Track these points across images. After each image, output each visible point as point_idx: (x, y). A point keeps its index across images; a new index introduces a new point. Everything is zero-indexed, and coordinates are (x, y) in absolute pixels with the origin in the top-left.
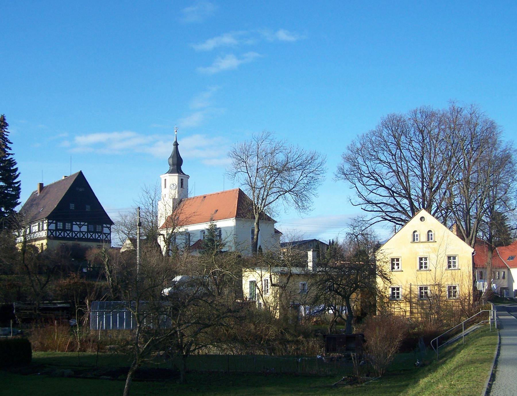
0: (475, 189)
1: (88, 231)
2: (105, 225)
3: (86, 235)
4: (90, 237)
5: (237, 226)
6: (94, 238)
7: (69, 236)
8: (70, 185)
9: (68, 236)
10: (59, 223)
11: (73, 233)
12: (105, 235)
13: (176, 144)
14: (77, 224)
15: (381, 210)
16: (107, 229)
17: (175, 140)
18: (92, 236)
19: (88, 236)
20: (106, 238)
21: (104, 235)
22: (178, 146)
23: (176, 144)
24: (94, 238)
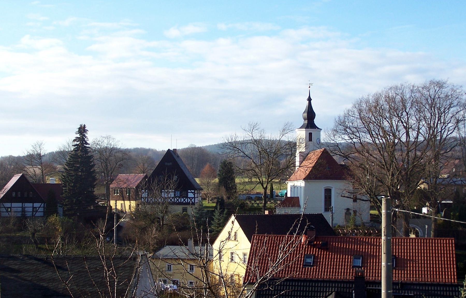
0: (434, 99)
1: (175, 197)
2: (189, 191)
3: (173, 200)
4: (183, 201)
5: (305, 187)
6: (180, 202)
7: (185, 201)
8: (14, 183)
9: (184, 202)
10: (177, 192)
11: (189, 199)
12: (190, 199)
13: (310, 99)
14: (191, 192)
15: (415, 149)
16: (192, 193)
17: (308, 96)
18: (184, 200)
19: (181, 201)
20: (152, 199)
21: (189, 199)
22: (311, 101)
23: (310, 99)
24: (180, 202)
